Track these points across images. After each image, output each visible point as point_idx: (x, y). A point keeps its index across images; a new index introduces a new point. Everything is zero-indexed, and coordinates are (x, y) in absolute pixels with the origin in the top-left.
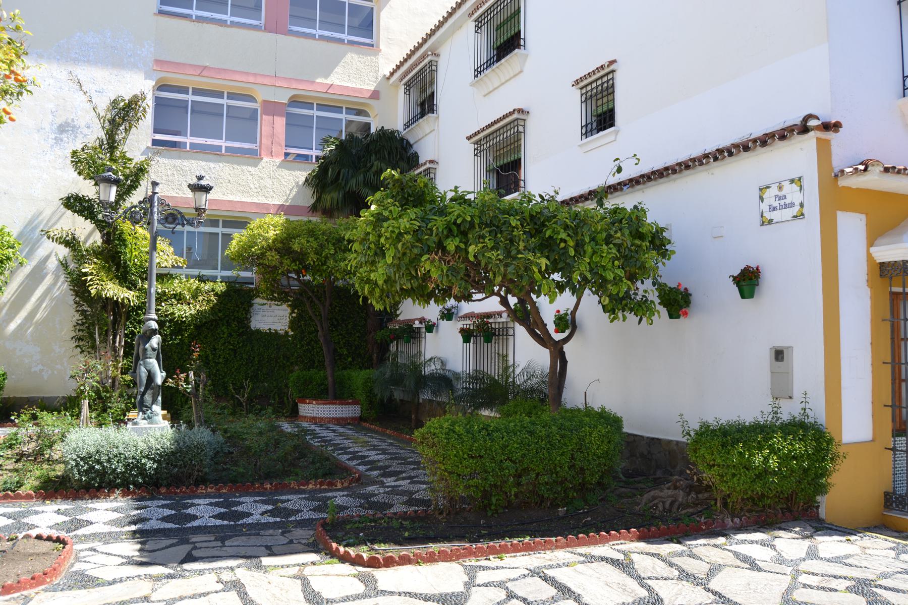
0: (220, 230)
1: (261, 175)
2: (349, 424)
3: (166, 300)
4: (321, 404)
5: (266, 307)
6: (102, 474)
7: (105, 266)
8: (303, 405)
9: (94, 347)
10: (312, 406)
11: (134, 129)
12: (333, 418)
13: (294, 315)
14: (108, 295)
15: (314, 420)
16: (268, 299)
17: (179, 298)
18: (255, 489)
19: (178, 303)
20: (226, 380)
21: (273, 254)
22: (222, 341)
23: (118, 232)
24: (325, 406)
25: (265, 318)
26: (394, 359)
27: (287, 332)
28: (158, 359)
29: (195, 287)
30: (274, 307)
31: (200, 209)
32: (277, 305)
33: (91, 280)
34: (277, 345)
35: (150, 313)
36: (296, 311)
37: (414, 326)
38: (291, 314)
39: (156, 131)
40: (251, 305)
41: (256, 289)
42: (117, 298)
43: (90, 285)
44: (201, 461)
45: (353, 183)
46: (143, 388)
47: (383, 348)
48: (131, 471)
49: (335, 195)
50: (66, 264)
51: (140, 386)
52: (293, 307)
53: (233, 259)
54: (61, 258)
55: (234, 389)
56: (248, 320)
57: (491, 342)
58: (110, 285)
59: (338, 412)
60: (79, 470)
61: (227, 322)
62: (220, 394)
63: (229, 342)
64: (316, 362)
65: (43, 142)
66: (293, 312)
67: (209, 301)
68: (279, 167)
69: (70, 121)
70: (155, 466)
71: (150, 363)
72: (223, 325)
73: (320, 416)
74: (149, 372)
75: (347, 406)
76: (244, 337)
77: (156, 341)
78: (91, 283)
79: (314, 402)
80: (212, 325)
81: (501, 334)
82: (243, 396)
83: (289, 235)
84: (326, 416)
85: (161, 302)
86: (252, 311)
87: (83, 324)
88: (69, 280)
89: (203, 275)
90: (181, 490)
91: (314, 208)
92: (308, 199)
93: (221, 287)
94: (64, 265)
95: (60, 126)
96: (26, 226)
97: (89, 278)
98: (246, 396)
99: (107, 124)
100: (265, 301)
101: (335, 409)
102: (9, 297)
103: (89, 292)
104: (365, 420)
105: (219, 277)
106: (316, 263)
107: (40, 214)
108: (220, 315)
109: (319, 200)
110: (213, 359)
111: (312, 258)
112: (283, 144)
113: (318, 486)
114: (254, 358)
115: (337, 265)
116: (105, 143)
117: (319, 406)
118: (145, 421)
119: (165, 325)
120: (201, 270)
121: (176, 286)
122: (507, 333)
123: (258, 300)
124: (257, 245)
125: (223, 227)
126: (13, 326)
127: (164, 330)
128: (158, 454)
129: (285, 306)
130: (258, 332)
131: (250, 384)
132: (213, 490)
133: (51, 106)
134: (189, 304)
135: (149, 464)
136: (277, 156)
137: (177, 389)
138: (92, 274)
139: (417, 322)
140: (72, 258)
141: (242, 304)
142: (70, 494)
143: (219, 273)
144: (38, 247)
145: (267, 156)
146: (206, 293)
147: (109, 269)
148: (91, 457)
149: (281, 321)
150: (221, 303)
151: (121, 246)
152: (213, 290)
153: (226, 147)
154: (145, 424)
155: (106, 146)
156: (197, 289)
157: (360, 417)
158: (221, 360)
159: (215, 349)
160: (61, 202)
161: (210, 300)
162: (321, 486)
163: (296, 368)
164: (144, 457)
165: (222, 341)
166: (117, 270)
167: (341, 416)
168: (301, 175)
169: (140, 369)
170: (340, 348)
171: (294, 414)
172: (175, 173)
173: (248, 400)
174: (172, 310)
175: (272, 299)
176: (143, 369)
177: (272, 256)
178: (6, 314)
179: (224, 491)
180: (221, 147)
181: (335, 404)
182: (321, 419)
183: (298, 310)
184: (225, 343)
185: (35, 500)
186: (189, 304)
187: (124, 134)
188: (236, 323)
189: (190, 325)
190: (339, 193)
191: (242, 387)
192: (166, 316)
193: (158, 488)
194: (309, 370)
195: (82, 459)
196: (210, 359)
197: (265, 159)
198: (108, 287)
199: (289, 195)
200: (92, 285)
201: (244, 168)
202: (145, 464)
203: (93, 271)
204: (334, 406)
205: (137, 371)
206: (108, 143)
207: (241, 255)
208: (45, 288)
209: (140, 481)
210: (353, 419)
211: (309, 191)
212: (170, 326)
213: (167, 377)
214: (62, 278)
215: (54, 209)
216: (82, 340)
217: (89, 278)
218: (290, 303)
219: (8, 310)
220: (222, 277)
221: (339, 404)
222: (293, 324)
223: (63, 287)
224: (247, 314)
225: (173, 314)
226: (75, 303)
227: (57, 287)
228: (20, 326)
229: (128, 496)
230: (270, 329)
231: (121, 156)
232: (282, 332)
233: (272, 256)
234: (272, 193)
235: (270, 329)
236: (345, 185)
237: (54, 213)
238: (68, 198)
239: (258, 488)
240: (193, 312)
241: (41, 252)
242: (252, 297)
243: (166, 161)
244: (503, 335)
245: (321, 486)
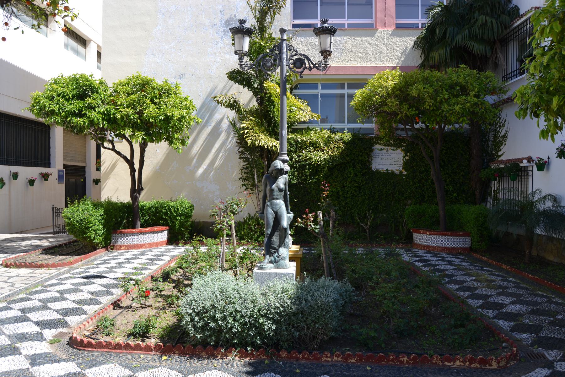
0: (346, 91)
1: (377, 43)
2: (460, 254)
3: (306, 148)
4: (434, 235)
5: (384, 151)
6: (219, 331)
7: (259, 122)
8: (418, 235)
9: (253, 185)
10: (425, 236)
11: (277, 16)
12: (445, 248)
13: (407, 158)
14: (260, 144)
15: (428, 249)
16: (385, 145)
17: (315, 146)
18: (389, 361)
19: (315, 150)
20: (353, 211)
21: (393, 100)
22: (349, 180)
23: (268, 95)
24: (438, 237)
25: (383, 161)
26: (495, 195)
27: (401, 172)
28: (285, 201)
29: (327, 136)
30: (390, 151)
31: (326, 51)
32: (393, 150)
33: (247, 133)
34: (393, 182)
35: (282, 154)
36: (408, 154)
37: (521, 165)
38: (404, 157)
39: (295, 17)
40: (372, 150)
41: (375, 137)
42: (268, 146)
43: (247, 137)
44: (326, 324)
45: (459, 39)
46: (270, 230)
47: (486, 185)
48: (248, 331)
49: (442, 51)
50: (235, 124)
51: (267, 228)
52: (406, 151)
53: (356, 109)
54: (231, 119)
55: (359, 219)
56: (370, 162)
57: (516, 180)
58: (262, 136)
59: (449, 243)
60: (194, 326)
61: (353, 164)
62: (348, 222)
63: (355, 181)
64: (426, 197)
65: (215, 35)
66: (406, 155)
67: (339, 148)
68: (392, 35)
69: (233, 16)
70: (274, 328)
71: (277, 204)
72: (350, 167)
73: (433, 245)
74: (276, 213)
75: (458, 238)
76: (367, 177)
77: (282, 181)
78: (247, 135)
79: (428, 233)
80: (341, 167)
81: (523, 175)
82: (367, 224)
83: (406, 82)
84: (438, 245)
85: (303, 150)
86: (372, 155)
87: (247, 168)
88: (237, 135)
89: (334, 128)
90: (303, 356)
91: (422, 66)
92: (417, 60)
93: (347, 137)
94: (233, 124)
95: (227, 21)
96: (207, 97)
97: (246, 131)
98: (369, 224)
99: (257, 13)
100: (383, 147)
101: (446, 240)
102: (198, 150)
103: (246, 142)
104: (475, 251)
105: (346, 129)
106: (432, 109)
107: (216, 88)
108: (347, 159)
109: (426, 59)
110: (343, 194)
111: (428, 104)
112: (394, 15)
113: (468, 363)
114: (375, 193)
115: (451, 108)
116: (257, 28)
117: (432, 236)
118: (272, 265)
119: (305, 168)
120: (332, 124)
121: (312, 136)
122: (527, 174)
123: (377, 146)
124: (379, 95)
125: (348, 89)
126: (200, 171)
127: (305, 172)
128: (277, 313)
129: (399, 151)
130: (378, 172)
131: (372, 214)
132: (340, 359)
133: (220, 7)
134: (323, 151)
135: (268, 325)
136: (390, 26)
137: (306, 229)
138: (248, 128)
139: (525, 161)
140: (238, 119)
141: (365, 149)
142: (188, 350)
143: (346, 126)
144: (216, 112)
145: (382, 27)
146: (336, 141)
147: (262, 124)
148: (206, 312)
149: (396, 163)
150: (348, 149)
151: (270, 106)
152: (341, 139)
153: (348, 24)
154: (271, 268)
155: (258, 31)
156: (329, 137)
157: (470, 247)
158: (349, 195)
159: (344, 187)
160: (227, 75)
161: (340, 147)
162: (471, 363)
163: (410, 202)
164: (262, 316)
165: (349, 180)
166: (269, 125)
167: (452, 246)
168: (410, 41)
169: (267, 210)
170: (447, 185)
171: (408, 241)
172: (310, 48)
173: (370, 227)
174: (310, 155)
175: (388, 146)
176: (270, 211)
177: (392, 102)
178: (196, 162)
179: (352, 361)
180: (344, 24)
181: (447, 235)
182: (434, 248)
183: (410, 154)
184: (351, 182)
185: (153, 353)
186: (323, 151)
187: (270, 19)
188: (360, 165)
189: (324, 168)
190: (446, 50)
191: (366, 217)
192: (306, 160)
193: (279, 351)
194: (420, 204)
195: (198, 314)
196: (340, 194)
197: (380, 30)
198: (260, 138)
199: (401, 57)
200: (248, 137)
201: (363, 38)
202: (262, 324)
203: (249, 126)
204: (446, 237)
205: (265, 212)
206: (259, 29)
207: (364, 105)
208: (221, 142)
209: (259, 342)
210: (464, 249)
211: (418, 52)
212: (309, 169)
213: (295, 218)
214: (232, 135)
215: (225, 83)
216: (247, 180)
217: (246, 131)
218: (403, 148)
219: (197, 159)
220: (348, 129)
221: (451, 235)
222: (406, 165)
223: (233, 140)
224: (369, 158)
225: (311, 158)
226: (239, 152)
227: (229, 141)
228: (206, 171)
229: (246, 357)
230: (387, 170)
231: (269, 37)
232: (397, 172)
233: (392, 102)
234: (386, 58)
235: (387, 170)
236: (452, 42)
237: (224, 87)
238: (232, 73)
239: (393, 360)
240: (327, 157)
241: (217, 116)
242: (373, 144)
243: (302, 39)
244: (524, 176)
245: (471, 363)
